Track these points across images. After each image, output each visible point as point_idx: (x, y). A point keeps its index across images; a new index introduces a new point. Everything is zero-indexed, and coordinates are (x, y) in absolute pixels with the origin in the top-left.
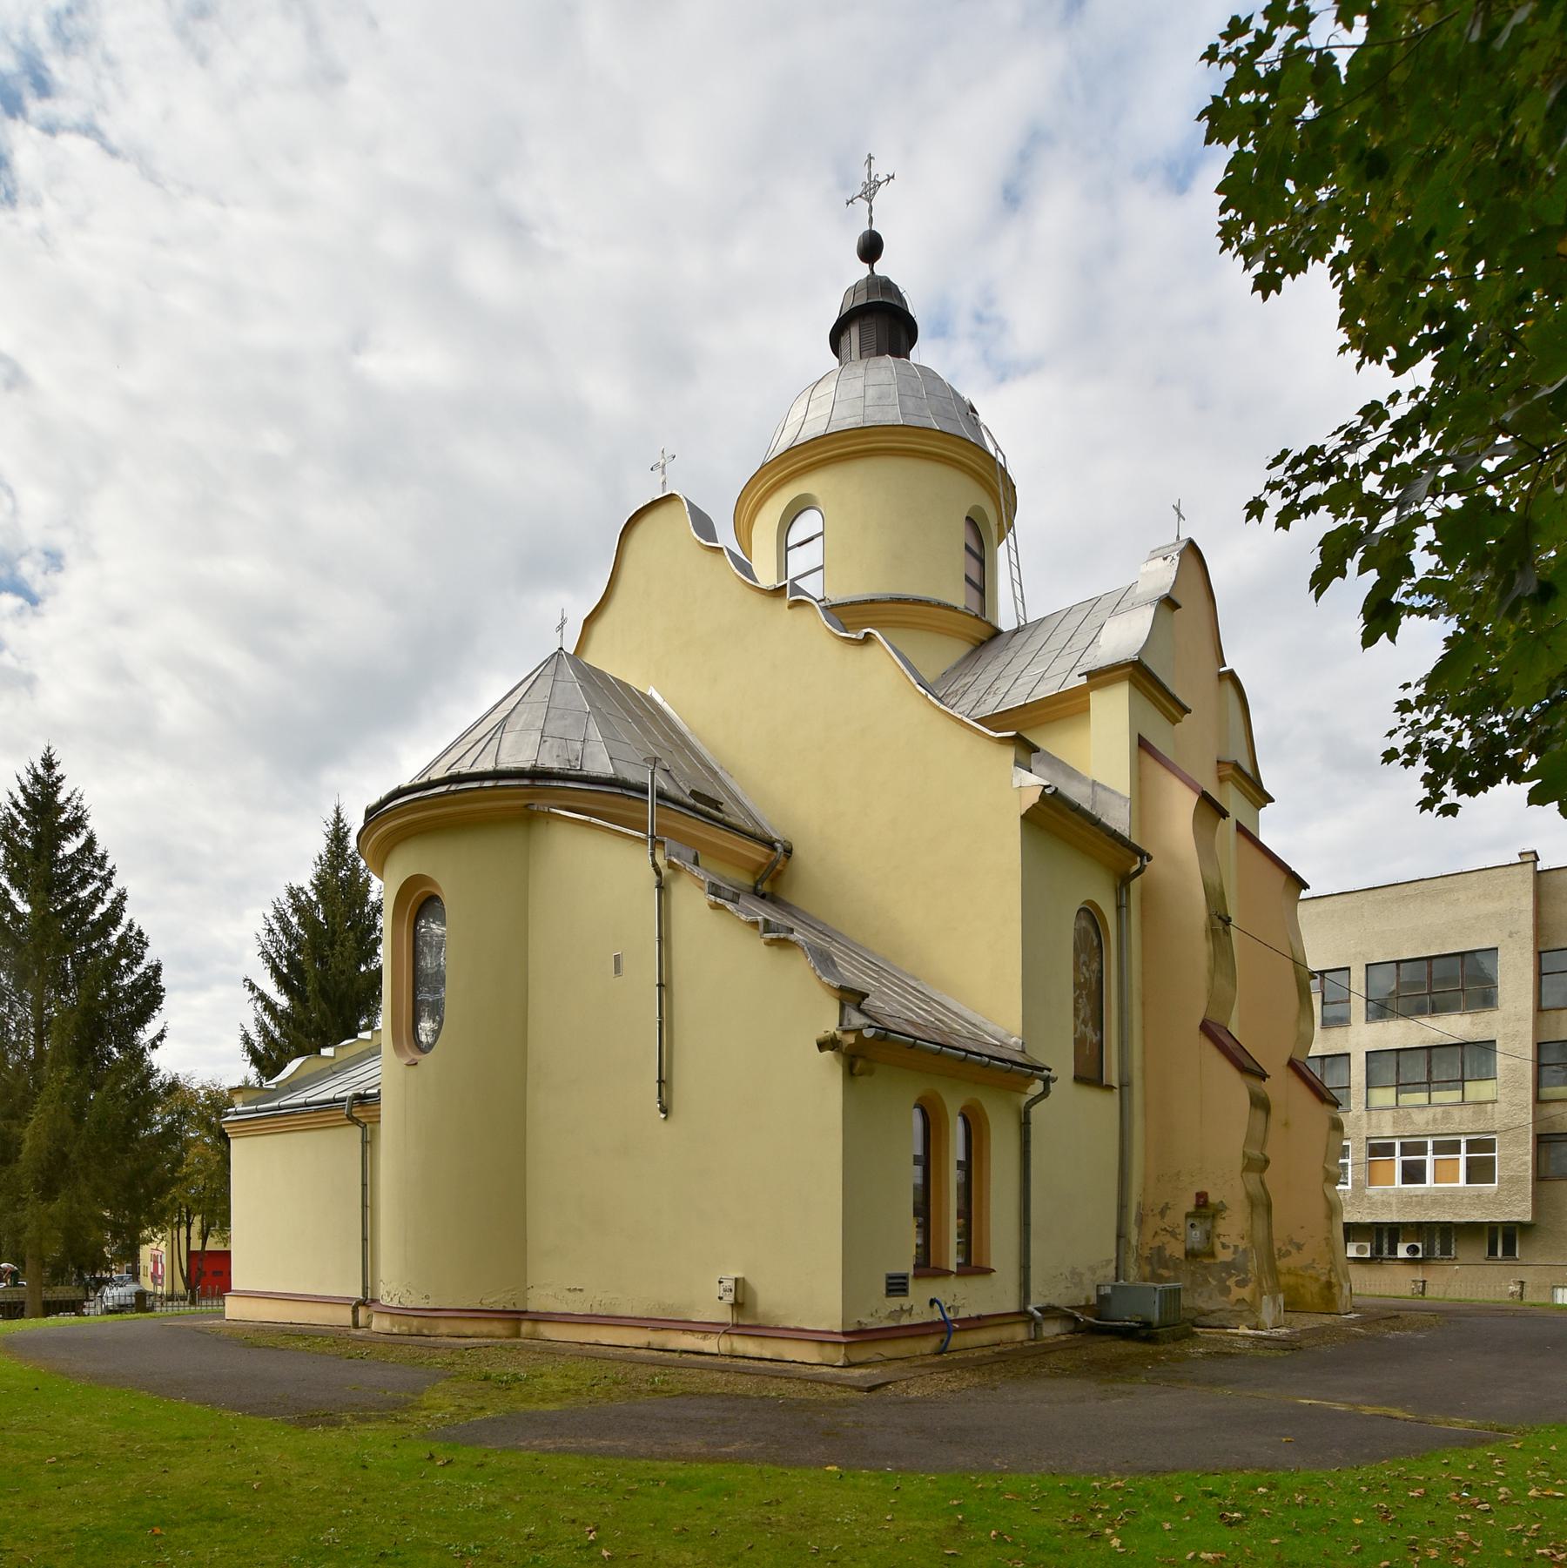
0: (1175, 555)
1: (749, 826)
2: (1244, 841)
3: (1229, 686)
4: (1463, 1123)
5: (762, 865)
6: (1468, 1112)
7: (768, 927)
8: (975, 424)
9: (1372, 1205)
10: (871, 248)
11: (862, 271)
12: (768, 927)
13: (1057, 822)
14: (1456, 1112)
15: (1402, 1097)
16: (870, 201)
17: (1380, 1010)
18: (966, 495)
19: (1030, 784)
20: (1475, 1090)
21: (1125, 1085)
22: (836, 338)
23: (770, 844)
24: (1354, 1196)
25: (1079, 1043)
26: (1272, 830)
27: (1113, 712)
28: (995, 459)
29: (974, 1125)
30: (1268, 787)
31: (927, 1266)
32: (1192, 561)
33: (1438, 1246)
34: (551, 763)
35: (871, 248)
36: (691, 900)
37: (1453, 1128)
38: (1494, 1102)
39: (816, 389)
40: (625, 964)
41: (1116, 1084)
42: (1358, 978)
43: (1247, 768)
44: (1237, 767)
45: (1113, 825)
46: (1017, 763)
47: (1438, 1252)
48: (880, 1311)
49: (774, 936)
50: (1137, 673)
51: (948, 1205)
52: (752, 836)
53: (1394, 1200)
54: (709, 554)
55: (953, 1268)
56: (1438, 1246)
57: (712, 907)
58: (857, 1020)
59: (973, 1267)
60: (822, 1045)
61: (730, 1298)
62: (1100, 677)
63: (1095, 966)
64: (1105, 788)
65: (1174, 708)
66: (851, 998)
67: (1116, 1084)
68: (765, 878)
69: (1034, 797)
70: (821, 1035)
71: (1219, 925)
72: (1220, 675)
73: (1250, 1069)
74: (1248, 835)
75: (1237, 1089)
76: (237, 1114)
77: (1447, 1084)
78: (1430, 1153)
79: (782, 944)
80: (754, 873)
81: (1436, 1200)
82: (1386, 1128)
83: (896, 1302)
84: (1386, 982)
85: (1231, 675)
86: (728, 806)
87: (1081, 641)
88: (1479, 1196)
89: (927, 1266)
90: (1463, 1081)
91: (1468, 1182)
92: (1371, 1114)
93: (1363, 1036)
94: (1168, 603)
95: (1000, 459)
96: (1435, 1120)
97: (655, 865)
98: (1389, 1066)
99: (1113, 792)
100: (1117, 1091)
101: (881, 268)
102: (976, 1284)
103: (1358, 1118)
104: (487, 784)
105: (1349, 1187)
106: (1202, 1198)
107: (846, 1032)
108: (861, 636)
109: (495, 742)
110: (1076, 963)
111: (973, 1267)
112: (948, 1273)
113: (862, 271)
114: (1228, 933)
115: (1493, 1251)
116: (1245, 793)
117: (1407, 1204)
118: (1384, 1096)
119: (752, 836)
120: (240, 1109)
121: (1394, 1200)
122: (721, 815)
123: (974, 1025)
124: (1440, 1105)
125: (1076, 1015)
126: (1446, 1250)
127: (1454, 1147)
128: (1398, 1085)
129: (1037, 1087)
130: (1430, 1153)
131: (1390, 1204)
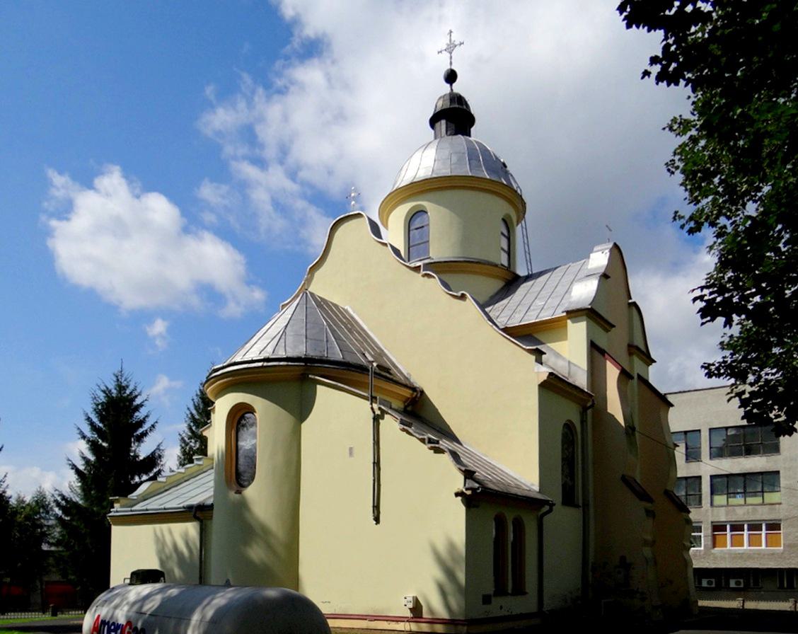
0: (607, 251)
1: (403, 380)
2: (643, 386)
3: (634, 309)
4: (763, 514)
5: (409, 398)
6: (766, 508)
7: (430, 441)
8: (506, 174)
9: (715, 558)
10: (451, 77)
11: (446, 89)
12: (430, 441)
13: (554, 386)
14: (759, 508)
15: (730, 500)
16: (451, 53)
17: (717, 453)
18: (502, 208)
19: (542, 373)
20: (769, 497)
21: (586, 506)
22: (433, 121)
23: (414, 389)
24: (705, 554)
25: (564, 486)
26: (654, 375)
27: (578, 332)
28: (516, 192)
29: (519, 526)
30: (653, 356)
31: (500, 590)
32: (616, 251)
33: (752, 581)
34: (312, 354)
35: (451, 77)
36: (391, 425)
37: (758, 517)
38: (780, 504)
39: (427, 158)
40: (355, 451)
41: (581, 504)
42: (705, 435)
43: (642, 348)
44: (638, 348)
45: (577, 384)
46: (536, 361)
47: (752, 584)
48: (480, 611)
49: (433, 445)
50: (590, 314)
51: (710, 599)
52: (405, 386)
53: (727, 556)
54: (380, 245)
55: (510, 591)
56: (752, 581)
57: (401, 430)
58: (471, 484)
59: (519, 590)
60: (457, 495)
61: (411, 605)
62: (574, 314)
63: (571, 450)
64: (575, 365)
65: (607, 325)
66: (469, 474)
67: (581, 504)
68: (418, 412)
69: (544, 377)
70: (456, 490)
71: (630, 432)
72: (630, 304)
73: (643, 495)
74: (644, 381)
75: (639, 507)
76: (117, 512)
77: (755, 494)
78: (746, 531)
79: (438, 451)
80: (405, 402)
81: (750, 556)
82: (722, 516)
83: (487, 607)
84: (719, 442)
85: (635, 304)
86: (394, 370)
87: (561, 290)
88: (773, 554)
89: (500, 590)
90: (763, 492)
91: (767, 546)
92: (706, 513)
93: (708, 467)
94: (605, 276)
95: (519, 191)
96: (748, 513)
97: (372, 409)
98: (724, 483)
99: (579, 367)
100: (581, 509)
101: (458, 88)
102: (520, 598)
103: (707, 511)
104: (282, 363)
105: (702, 548)
106: (623, 558)
107: (467, 489)
108: (459, 294)
109: (282, 340)
110: (563, 449)
111: (519, 590)
112: (508, 594)
113: (446, 89)
114: (634, 435)
115: (781, 586)
116: (642, 360)
117: (734, 558)
118: (720, 499)
119: (405, 386)
120: (119, 509)
121: (727, 556)
122: (391, 377)
123: (515, 479)
124: (751, 505)
125: (563, 474)
126: (756, 583)
127: (758, 528)
128: (728, 494)
129: (546, 508)
130: (746, 531)
131: (725, 558)
